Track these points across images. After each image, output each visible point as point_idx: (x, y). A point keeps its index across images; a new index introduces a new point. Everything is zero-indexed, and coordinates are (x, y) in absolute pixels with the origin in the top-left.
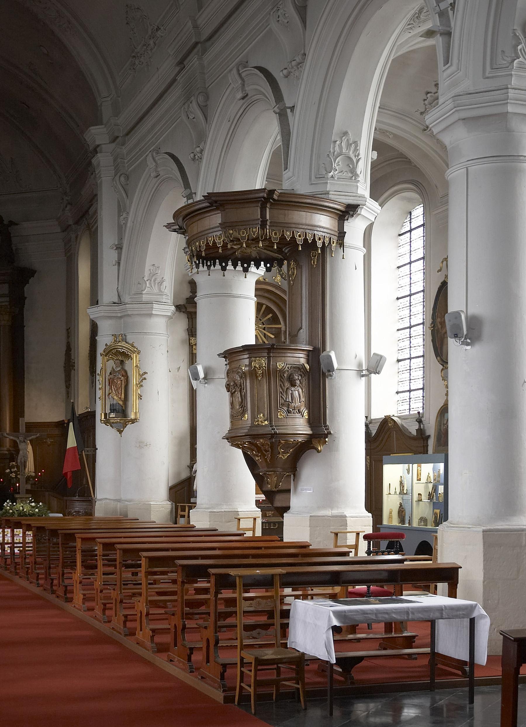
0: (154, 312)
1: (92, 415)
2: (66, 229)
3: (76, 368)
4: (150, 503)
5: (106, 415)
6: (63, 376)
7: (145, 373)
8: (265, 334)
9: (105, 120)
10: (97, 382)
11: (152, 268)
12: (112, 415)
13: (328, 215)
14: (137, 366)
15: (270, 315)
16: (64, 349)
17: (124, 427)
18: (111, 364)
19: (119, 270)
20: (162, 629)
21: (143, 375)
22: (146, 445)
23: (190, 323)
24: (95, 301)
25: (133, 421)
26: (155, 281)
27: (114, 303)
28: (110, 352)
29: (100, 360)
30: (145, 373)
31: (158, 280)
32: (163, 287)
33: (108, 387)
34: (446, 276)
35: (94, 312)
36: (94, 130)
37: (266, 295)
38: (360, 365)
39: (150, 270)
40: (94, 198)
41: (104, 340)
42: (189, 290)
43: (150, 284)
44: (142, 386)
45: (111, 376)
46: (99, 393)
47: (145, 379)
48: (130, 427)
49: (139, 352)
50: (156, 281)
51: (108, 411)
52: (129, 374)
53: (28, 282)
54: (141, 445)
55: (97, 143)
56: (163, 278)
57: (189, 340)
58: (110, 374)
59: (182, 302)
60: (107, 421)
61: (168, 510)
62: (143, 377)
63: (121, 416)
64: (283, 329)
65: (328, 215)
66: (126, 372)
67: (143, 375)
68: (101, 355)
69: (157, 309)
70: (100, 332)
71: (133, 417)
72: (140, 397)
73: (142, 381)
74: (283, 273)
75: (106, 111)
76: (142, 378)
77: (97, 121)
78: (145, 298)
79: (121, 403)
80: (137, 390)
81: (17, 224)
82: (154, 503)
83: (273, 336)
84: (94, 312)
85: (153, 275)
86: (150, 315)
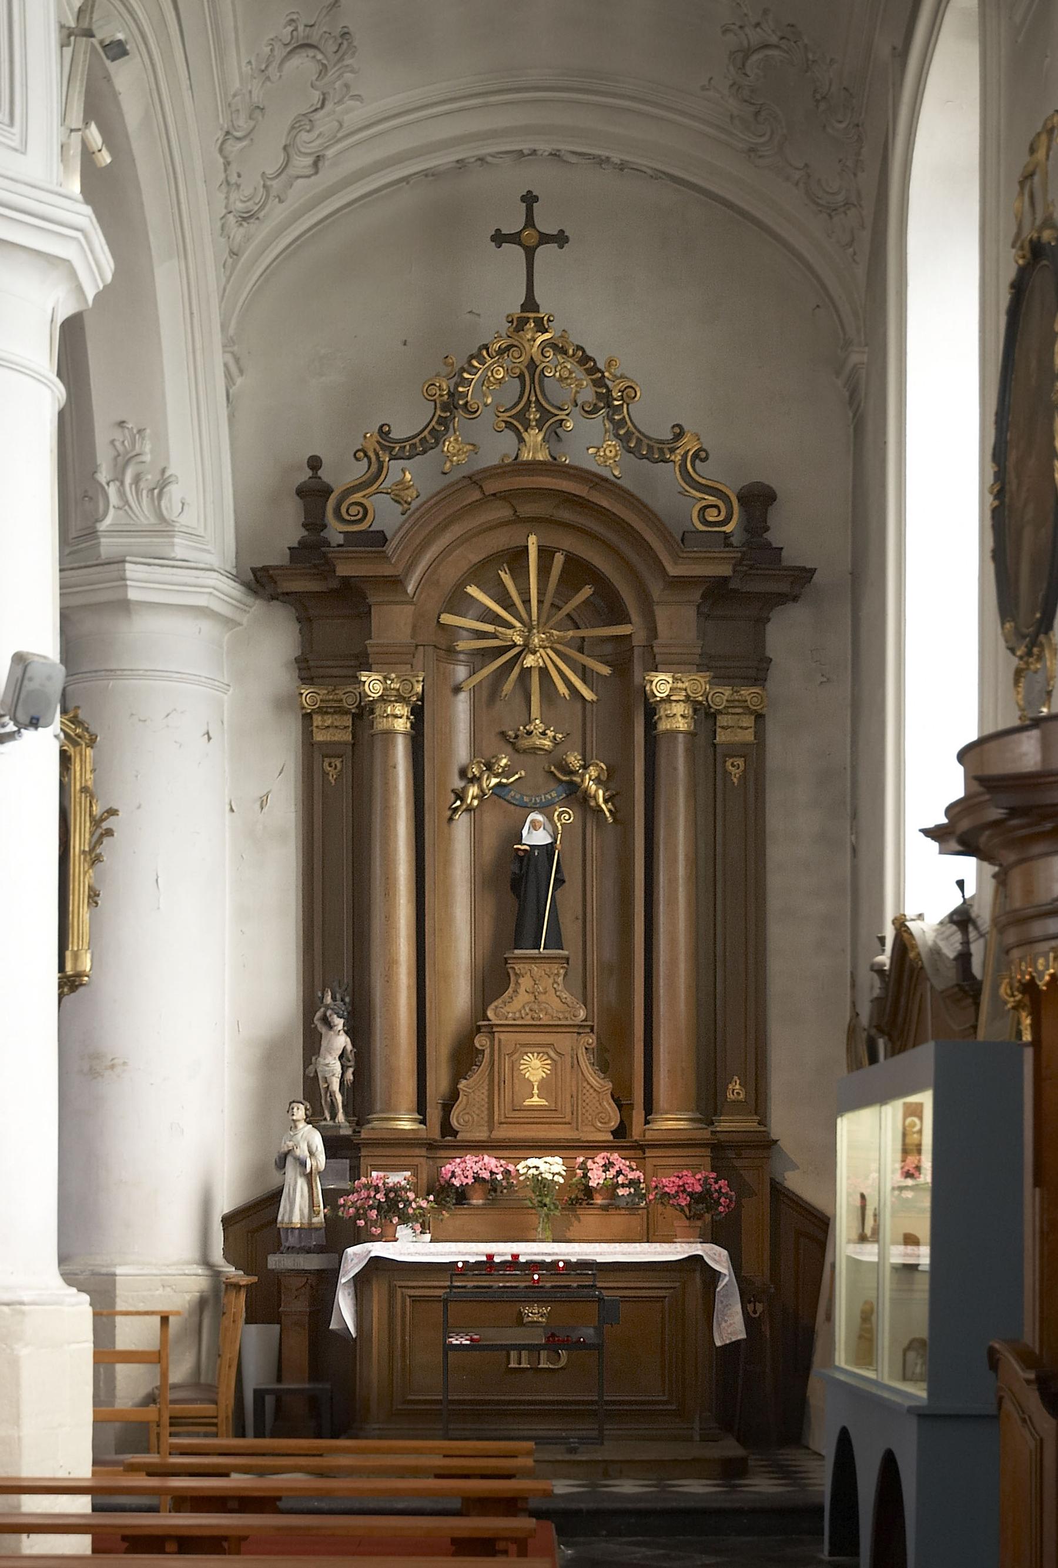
4: (112, 1270)
7: (112, 812)
8: (584, 666)
11: (118, 435)
13: (1044, 908)
15: (587, 591)
20: (466, 1439)
22: (112, 1067)
26: (137, 479)
31: (150, 478)
34: (903, 1161)
37: (566, 515)
39: (112, 442)
43: (122, 494)
47: (109, 833)
49: (92, 743)
50: (142, 485)
56: (163, 471)
61: (188, 1297)
62: (105, 825)
64: (639, 639)
65: (1044, 908)
67: (102, 820)
72: (93, 896)
73: (99, 842)
74: (629, 434)
76: (99, 831)
83: (606, 670)
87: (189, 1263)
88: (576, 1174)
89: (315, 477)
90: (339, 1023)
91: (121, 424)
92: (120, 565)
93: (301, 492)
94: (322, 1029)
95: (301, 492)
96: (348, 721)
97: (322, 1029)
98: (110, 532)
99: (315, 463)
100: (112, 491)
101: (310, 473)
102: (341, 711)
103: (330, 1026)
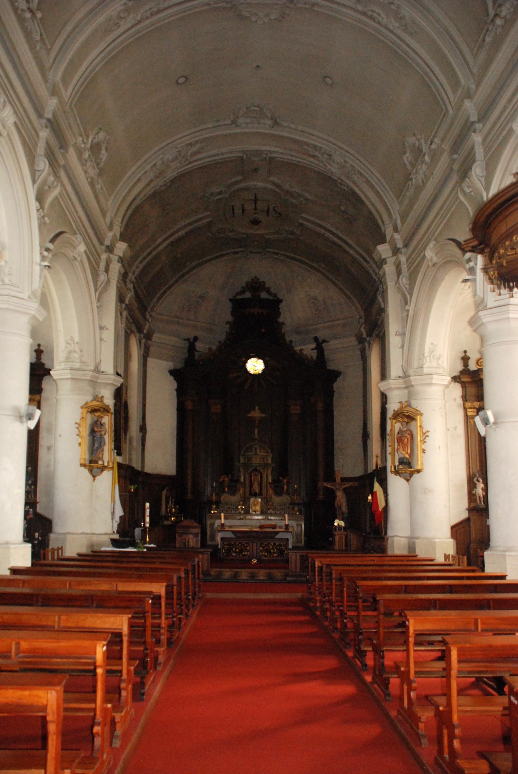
0: (434, 382)
1: (384, 469)
2: (361, 340)
3: (370, 438)
5: (395, 467)
6: (361, 443)
9: (388, 238)
10: (388, 441)
12: (401, 467)
14: (420, 426)
16: (362, 425)
17: (411, 477)
18: (398, 426)
19: (403, 353)
21: (425, 433)
23: (464, 391)
24: (384, 376)
25: (418, 471)
27: (400, 377)
28: (397, 415)
29: (389, 422)
30: (428, 431)
32: (440, 362)
33: (396, 444)
35: (383, 386)
36: (381, 248)
38: (417, 538)
40: (382, 311)
41: (393, 406)
42: (462, 364)
44: (425, 442)
45: (400, 435)
46: (389, 450)
47: (427, 436)
48: (416, 476)
51: (397, 463)
52: (414, 433)
53: (336, 381)
54: (426, 491)
55: (383, 257)
57: (464, 404)
58: (398, 433)
59: (457, 374)
60: (397, 472)
62: (426, 434)
63: (408, 468)
66: (411, 432)
67: (425, 433)
68: (390, 419)
69: (436, 379)
70: (389, 400)
71: (419, 468)
72: (424, 451)
73: (425, 438)
75: (389, 232)
77: (382, 240)
78: (426, 370)
79: (407, 456)
80: (421, 446)
81: (328, 342)
82: (438, 543)
84: (383, 386)
85: (431, 352)
86: (431, 384)
87: (448, 538)
88: (189, 599)
89: (466, 355)
90: (481, 480)
91: (432, 344)
92: (92, 379)
93: (36, 351)
94: (477, 482)
95: (36, 351)
96: (475, 410)
97: (477, 482)
98: (427, 367)
99: (465, 352)
100: (428, 358)
101: (464, 354)
102: (475, 408)
103: (478, 481)
